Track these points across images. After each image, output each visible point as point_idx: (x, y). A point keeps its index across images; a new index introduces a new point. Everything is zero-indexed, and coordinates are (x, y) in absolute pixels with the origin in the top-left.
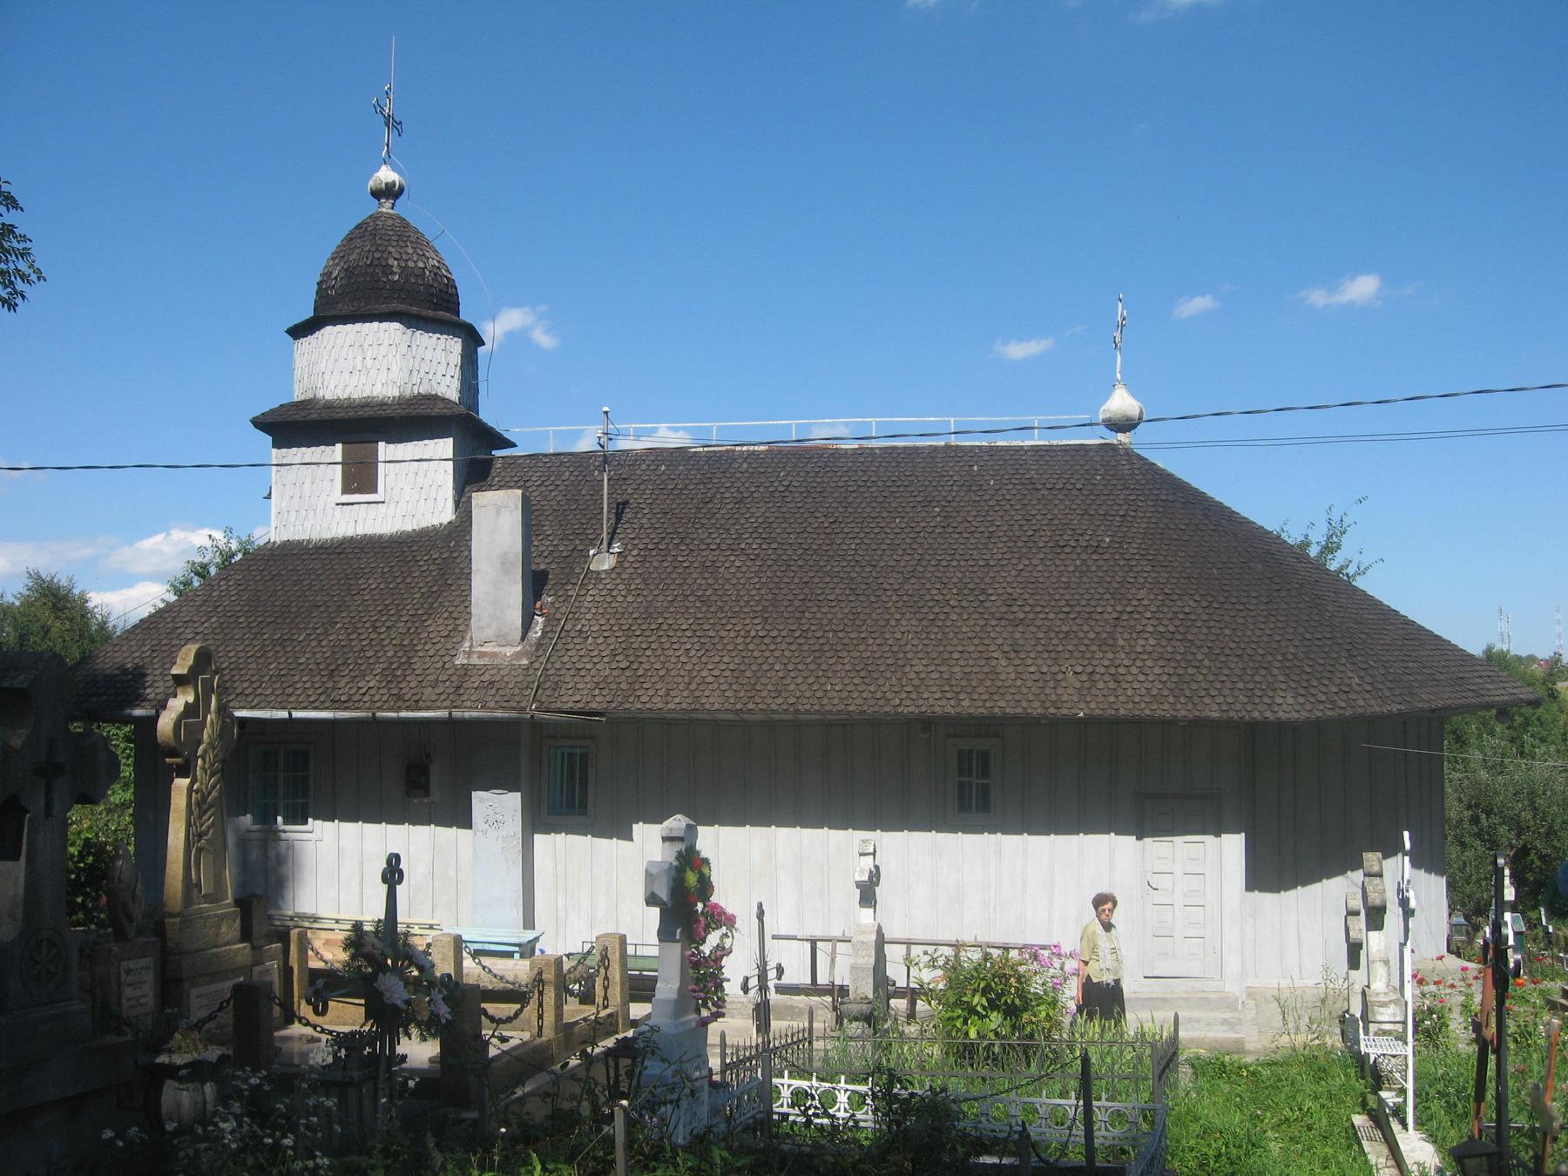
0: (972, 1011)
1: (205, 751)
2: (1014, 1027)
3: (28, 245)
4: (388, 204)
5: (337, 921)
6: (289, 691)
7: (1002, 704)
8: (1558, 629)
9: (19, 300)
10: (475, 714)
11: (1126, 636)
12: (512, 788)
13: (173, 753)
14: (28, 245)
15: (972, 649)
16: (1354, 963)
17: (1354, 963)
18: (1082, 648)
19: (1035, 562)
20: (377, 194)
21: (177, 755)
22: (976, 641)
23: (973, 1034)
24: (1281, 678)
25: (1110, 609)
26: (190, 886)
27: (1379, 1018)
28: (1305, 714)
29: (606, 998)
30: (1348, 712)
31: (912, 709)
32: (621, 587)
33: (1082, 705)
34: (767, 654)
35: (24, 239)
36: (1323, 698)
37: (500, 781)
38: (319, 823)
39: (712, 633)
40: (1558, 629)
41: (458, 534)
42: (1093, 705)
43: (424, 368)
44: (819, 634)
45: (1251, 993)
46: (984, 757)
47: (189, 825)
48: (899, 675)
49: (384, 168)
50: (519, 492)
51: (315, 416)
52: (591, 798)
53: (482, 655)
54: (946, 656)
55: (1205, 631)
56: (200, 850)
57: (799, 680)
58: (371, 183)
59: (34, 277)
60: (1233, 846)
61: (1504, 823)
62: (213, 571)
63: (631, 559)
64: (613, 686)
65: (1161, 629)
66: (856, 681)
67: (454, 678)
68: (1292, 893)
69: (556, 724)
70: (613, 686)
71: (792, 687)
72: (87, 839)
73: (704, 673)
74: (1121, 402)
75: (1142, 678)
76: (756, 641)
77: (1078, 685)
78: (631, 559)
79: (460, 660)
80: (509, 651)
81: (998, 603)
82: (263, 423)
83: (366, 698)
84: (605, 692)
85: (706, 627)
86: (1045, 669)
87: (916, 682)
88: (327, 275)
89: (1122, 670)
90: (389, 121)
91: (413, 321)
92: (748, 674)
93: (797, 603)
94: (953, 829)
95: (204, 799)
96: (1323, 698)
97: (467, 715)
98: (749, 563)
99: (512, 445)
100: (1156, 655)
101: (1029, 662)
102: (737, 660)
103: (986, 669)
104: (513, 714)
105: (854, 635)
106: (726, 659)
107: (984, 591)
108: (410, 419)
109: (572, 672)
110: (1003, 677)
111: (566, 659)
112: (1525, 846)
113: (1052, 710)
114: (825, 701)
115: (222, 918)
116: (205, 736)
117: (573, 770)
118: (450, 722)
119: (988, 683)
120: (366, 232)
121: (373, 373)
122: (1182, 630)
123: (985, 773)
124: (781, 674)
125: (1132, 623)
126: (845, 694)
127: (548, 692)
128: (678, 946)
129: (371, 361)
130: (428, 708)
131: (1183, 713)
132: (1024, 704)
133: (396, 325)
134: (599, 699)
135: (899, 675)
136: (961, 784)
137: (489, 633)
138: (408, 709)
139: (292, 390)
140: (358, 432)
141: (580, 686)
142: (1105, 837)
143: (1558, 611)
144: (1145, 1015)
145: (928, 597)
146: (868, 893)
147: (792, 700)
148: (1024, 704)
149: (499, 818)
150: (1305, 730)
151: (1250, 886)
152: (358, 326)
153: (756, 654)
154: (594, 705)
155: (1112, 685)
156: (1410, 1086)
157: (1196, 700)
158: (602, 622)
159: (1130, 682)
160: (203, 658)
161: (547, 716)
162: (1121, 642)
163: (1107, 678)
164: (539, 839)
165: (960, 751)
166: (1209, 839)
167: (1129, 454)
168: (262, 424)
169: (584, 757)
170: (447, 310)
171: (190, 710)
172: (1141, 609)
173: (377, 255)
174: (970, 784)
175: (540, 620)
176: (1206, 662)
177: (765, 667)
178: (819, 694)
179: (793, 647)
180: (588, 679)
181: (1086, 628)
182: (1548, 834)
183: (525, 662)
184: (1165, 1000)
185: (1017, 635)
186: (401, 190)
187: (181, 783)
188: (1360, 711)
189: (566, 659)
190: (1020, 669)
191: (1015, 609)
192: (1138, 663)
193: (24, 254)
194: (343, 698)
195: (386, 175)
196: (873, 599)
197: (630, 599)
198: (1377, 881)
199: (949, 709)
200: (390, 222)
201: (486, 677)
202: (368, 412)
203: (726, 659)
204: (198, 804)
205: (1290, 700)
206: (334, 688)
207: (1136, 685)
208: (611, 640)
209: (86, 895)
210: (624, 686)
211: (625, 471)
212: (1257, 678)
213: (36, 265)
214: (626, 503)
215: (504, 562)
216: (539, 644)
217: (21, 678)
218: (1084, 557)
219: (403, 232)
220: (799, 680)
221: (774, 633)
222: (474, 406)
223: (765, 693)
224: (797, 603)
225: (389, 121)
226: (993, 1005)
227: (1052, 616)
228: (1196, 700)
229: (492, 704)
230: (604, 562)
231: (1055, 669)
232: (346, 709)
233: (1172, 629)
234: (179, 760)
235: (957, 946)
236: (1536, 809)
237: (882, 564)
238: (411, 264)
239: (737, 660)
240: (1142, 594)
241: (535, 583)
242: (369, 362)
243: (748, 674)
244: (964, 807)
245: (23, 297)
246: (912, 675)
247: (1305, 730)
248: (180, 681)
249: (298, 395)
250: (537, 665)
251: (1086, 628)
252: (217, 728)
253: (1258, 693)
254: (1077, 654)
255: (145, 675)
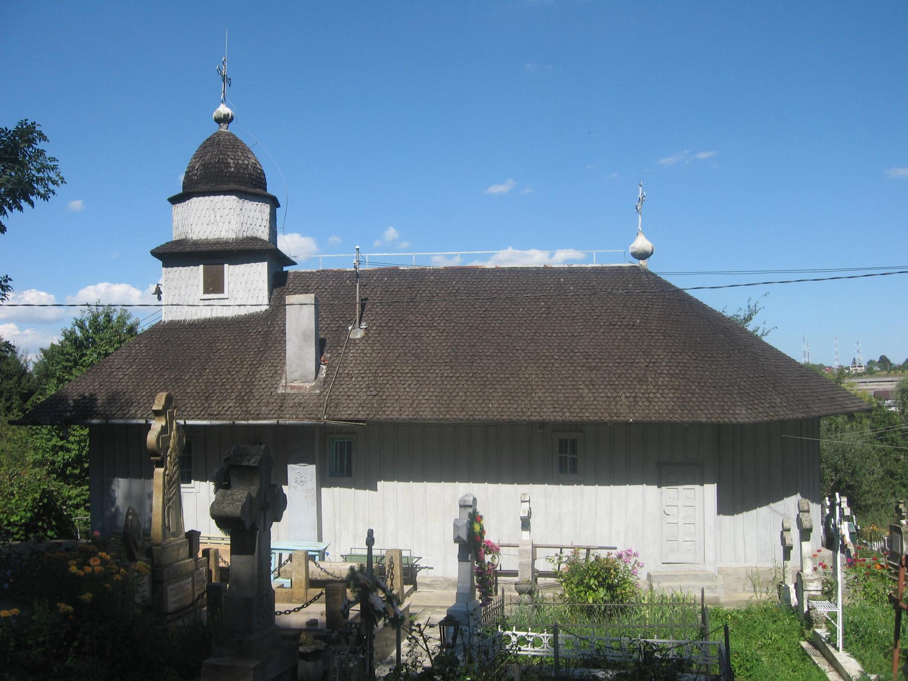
0: (590, 587)
1: (171, 452)
2: (612, 596)
3: (56, 163)
4: (225, 126)
5: (209, 538)
6: (183, 409)
7: (587, 414)
8: (836, 349)
9: (51, 195)
10: (292, 422)
11: (653, 376)
12: (310, 462)
13: (155, 454)
14: (56, 163)
15: (568, 383)
16: (787, 555)
17: (787, 555)
18: (629, 383)
19: (599, 334)
20: (219, 120)
21: (159, 456)
22: (570, 379)
23: (591, 601)
24: (738, 399)
25: (642, 361)
26: (165, 528)
27: (809, 588)
28: (753, 420)
29: (392, 585)
30: (776, 418)
31: (538, 418)
32: (369, 348)
33: (631, 415)
34: (454, 387)
35: (54, 159)
36: (761, 410)
37: (303, 459)
38: (198, 483)
39: (422, 375)
40: (836, 349)
41: (274, 317)
42: (637, 415)
43: (249, 222)
44: (483, 375)
45: (720, 571)
46: (574, 443)
47: (164, 495)
48: (529, 398)
49: (222, 105)
50: (313, 295)
51: (188, 249)
52: (354, 468)
53: (293, 388)
54: (554, 387)
55: (695, 373)
56: (169, 508)
57: (474, 402)
58: (215, 114)
59: (60, 182)
60: (710, 491)
61: (828, 467)
62: (87, 324)
63: (372, 332)
64: (369, 405)
65: (672, 372)
66: (506, 402)
67: (278, 401)
68: (740, 515)
69: (333, 427)
70: (369, 405)
71: (470, 405)
72: (44, 489)
73: (420, 398)
74: (642, 243)
75: (663, 399)
76: (448, 379)
77: (628, 403)
78: (372, 332)
79: (280, 391)
80: (308, 385)
81: (581, 357)
82: (156, 253)
83: (228, 413)
84: (365, 409)
85: (419, 371)
86: (609, 395)
87: (539, 403)
88: (191, 169)
89: (651, 395)
90: (224, 79)
91: (243, 195)
92: (445, 398)
93: (468, 357)
94: (557, 483)
95: (171, 479)
96: (761, 410)
97: (287, 422)
98: (440, 334)
99: (294, 263)
100: (670, 387)
101: (601, 391)
102: (438, 390)
103: (577, 395)
104: (314, 422)
105: (502, 376)
106: (432, 390)
107: (572, 351)
108: (244, 251)
109: (345, 397)
110: (587, 399)
111: (341, 390)
112: (840, 480)
113: (615, 418)
114: (489, 413)
115: (181, 545)
116: (171, 444)
117: (352, 453)
118: (278, 426)
119: (579, 403)
120: (212, 142)
121: (221, 224)
122: (683, 372)
123: (574, 452)
124: (463, 398)
125: (655, 368)
126: (500, 410)
127: (333, 409)
128: (469, 564)
129: (219, 218)
130: (265, 419)
131: (686, 419)
132: (600, 415)
133: (234, 197)
134: (362, 413)
135: (529, 398)
136: (561, 458)
137: (296, 375)
138: (253, 419)
139: (172, 234)
140: (213, 257)
141: (351, 405)
142: (640, 487)
143: (836, 339)
144: (665, 584)
145: (541, 354)
146: (526, 524)
147: (471, 413)
148: (600, 415)
149: (303, 479)
150: (746, 425)
151: (719, 513)
152: (212, 197)
153: (448, 387)
154: (359, 416)
155: (647, 403)
156: (840, 627)
157: (693, 412)
158: (360, 368)
159: (656, 402)
160: (169, 400)
161: (333, 423)
162: (650, 379)
163: (643, 400)
164: (324, 490)
165: (561, 440)
166: (697, 487)
167: (647, 273)
168: (156, 253)
169: (349, 444)
170: (260, 188)
171: (164, 430)
172: (660, 361)
173: (221, 157)
174: (566, 458)
175: (324, 367)
176: (697, 391)
177: (454, 394)
178: (486, 410)
179: (469, 383)
180: (354, 401)
181: (630, 371)
182: (852, 474)
183: (318, 391)
184: (675, 576)
185: (593, 376)
186: (232, 118)
187: (159, 471)
188: (782, 417)
189: (341, 390)
190: (596, 395)
191: (590, 361)
192: (660, 391)
193: (54, 168)
194: (215, 413)
195: (223, 110)
196: (511, 355)
197: (374, 355)
198: (807, 514)
199: (558, 418)
200: (227, 137)
201: (296, 401)
202: (219, 248)
203: (432, 390)
204: (168, 482)
205: (744, 412)
206: (209, 407)
207: (660, 404)
208: (366, 379)
209: (43, 521)
210: (375, 405)
211: (364, 281)
212: (726, 400)
213: (61, 175)
214: (366, 299)
215: (305, 336)
216: (325, 381)
217: (253, 460)
218: (626, 331)
219: (235, 144)
220: (474, 402)
221: (458, 375)
222: (275, 243)
223: (455, 409)
224: (468, 357)
225: (224, 79)
226: (601, 585)
227: (611, 365)
228: (693, 412)
229: (301, 416)
230: (358, 334)
231: (615, 395)
232: (217, 419)
233: (677, 372)
234: (158, 458)
235: (576, 549)
236: (845, 459)
237: (514, 335)
238: (240, 162)
239: (438, 390)
240: (660, 352)
241: (321, 345)
242: (218, 218)
243: (445, 398)
244: (562, 469)
245: (54, 193)
246: (537, 399)
247: (746, 425)
248: (157, 414)
249: (175, 236)
250: (325, 393)
251: (630, 371)
252: (177, 439)
253: (726, 407)
254: (626, 386)
255: (96, 400)
